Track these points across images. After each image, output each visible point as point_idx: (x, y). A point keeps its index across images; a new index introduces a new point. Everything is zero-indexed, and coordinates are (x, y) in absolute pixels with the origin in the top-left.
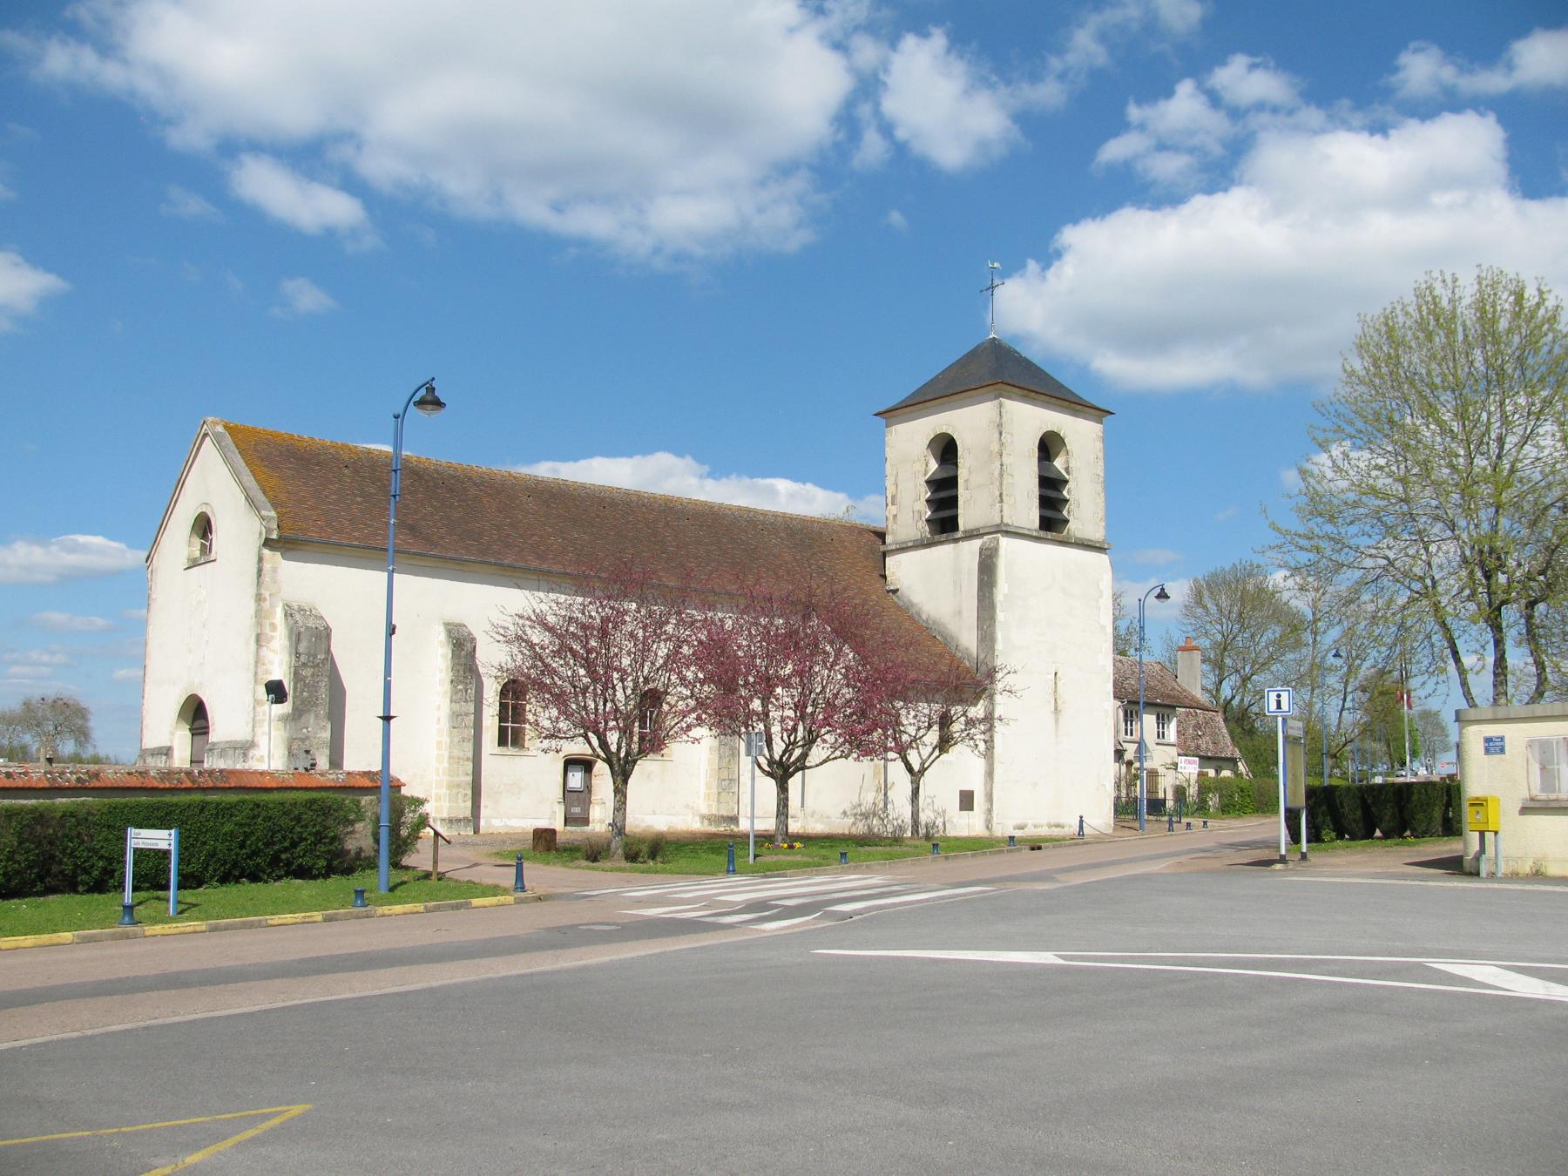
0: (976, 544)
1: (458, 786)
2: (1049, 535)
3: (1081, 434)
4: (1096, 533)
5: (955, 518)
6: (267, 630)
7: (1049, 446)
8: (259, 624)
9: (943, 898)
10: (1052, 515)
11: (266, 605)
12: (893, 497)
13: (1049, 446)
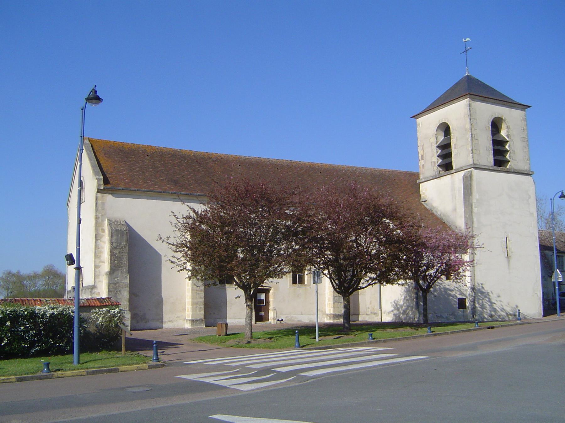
0: (462, 174)
1: (197, 303)
2: (499, 168)
3: (513, 119)
4: (523, 166)
5: (451, 163)
6: (100, 232)
7: (496, 125)
8: (97, 230)
9: (412, 360)
10: (500, 159)
11: (100, 220)
12: (422, 156)
13: (496, 125)
